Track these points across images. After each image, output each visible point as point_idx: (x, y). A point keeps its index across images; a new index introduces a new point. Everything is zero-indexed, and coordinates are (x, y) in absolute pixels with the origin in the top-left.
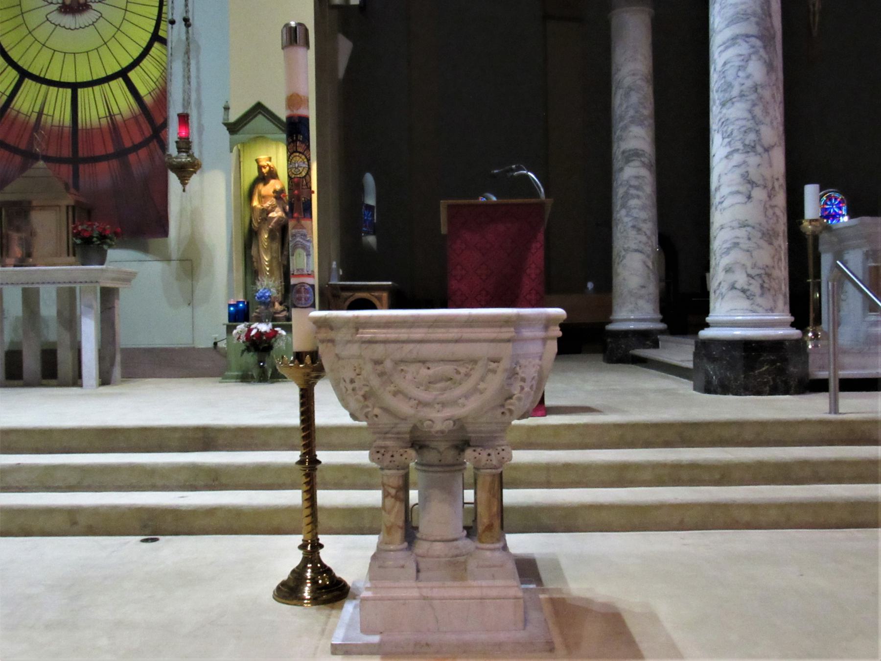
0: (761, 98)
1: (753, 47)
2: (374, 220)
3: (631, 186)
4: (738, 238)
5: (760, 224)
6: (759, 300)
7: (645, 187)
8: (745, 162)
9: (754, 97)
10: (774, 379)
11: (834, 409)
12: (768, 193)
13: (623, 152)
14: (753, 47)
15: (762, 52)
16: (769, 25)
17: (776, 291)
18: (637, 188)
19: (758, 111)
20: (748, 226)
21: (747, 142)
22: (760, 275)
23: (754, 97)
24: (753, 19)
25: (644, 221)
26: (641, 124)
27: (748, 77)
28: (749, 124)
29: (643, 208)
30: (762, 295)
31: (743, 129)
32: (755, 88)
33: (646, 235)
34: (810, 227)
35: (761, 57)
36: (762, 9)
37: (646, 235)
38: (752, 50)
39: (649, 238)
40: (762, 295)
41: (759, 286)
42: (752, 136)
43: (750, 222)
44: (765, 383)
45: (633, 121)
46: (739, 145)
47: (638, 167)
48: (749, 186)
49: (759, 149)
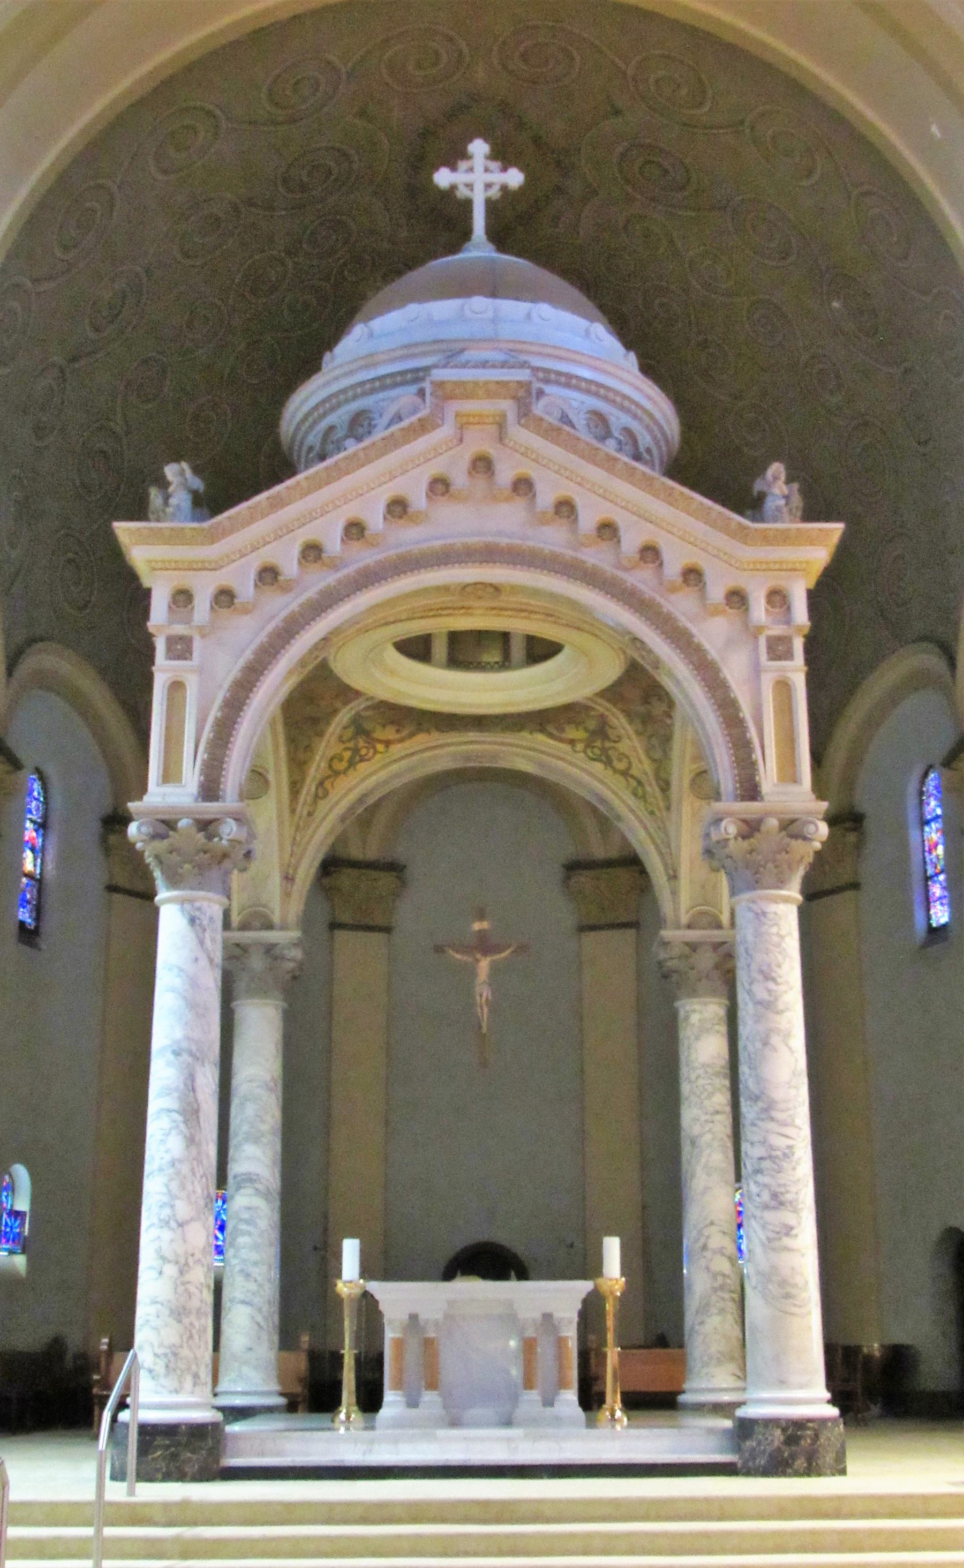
0: (178, 1173)
1: (174, 1121)
2: (24, 1232)
3: (241, 1220)
4: (148, 1314)
5: (169, 1301)
6: (163, 1381)
7: (259, 1221)
8: (159, 1237)
9: (171, 1171)
10: (167, 1467)
11: (131, 1492)
12: (180, 1269)
13: (235, 1177)
14: (174, 1121)
15: (182, 1126)
16: (192, 1099)
17: (182, 1371)
18: (247, 1222)
19: (174, 1186)
20: (158, 1302)
21: (162, 1217)
22: (166, 1355)
23: (171, 1171)
24: (176, 1094)
25: (256, 1264)
26: (256, 1141)
27: (167, 1151)
28: (165, 1199)
29: (255, 1247)
30: (167, 1375)
31: (160, 1204)
32: (173, 1163)
33: (256, 1281)
34: (345, 1289)
35: (181, 1132)
36: (186, 1085)
37: (256, 1281)
38: (174, 1124)
39: (260, 1286)
40: (167, 1375)
41: (164, 1366)
42: (167, 1212)
43: (159, 1299)
44: (157, 1470)
45: (247, 1140)
46: (156, 1220)
47: (250, 1195)
48: (161, 1262)
49: (173, 1224)
